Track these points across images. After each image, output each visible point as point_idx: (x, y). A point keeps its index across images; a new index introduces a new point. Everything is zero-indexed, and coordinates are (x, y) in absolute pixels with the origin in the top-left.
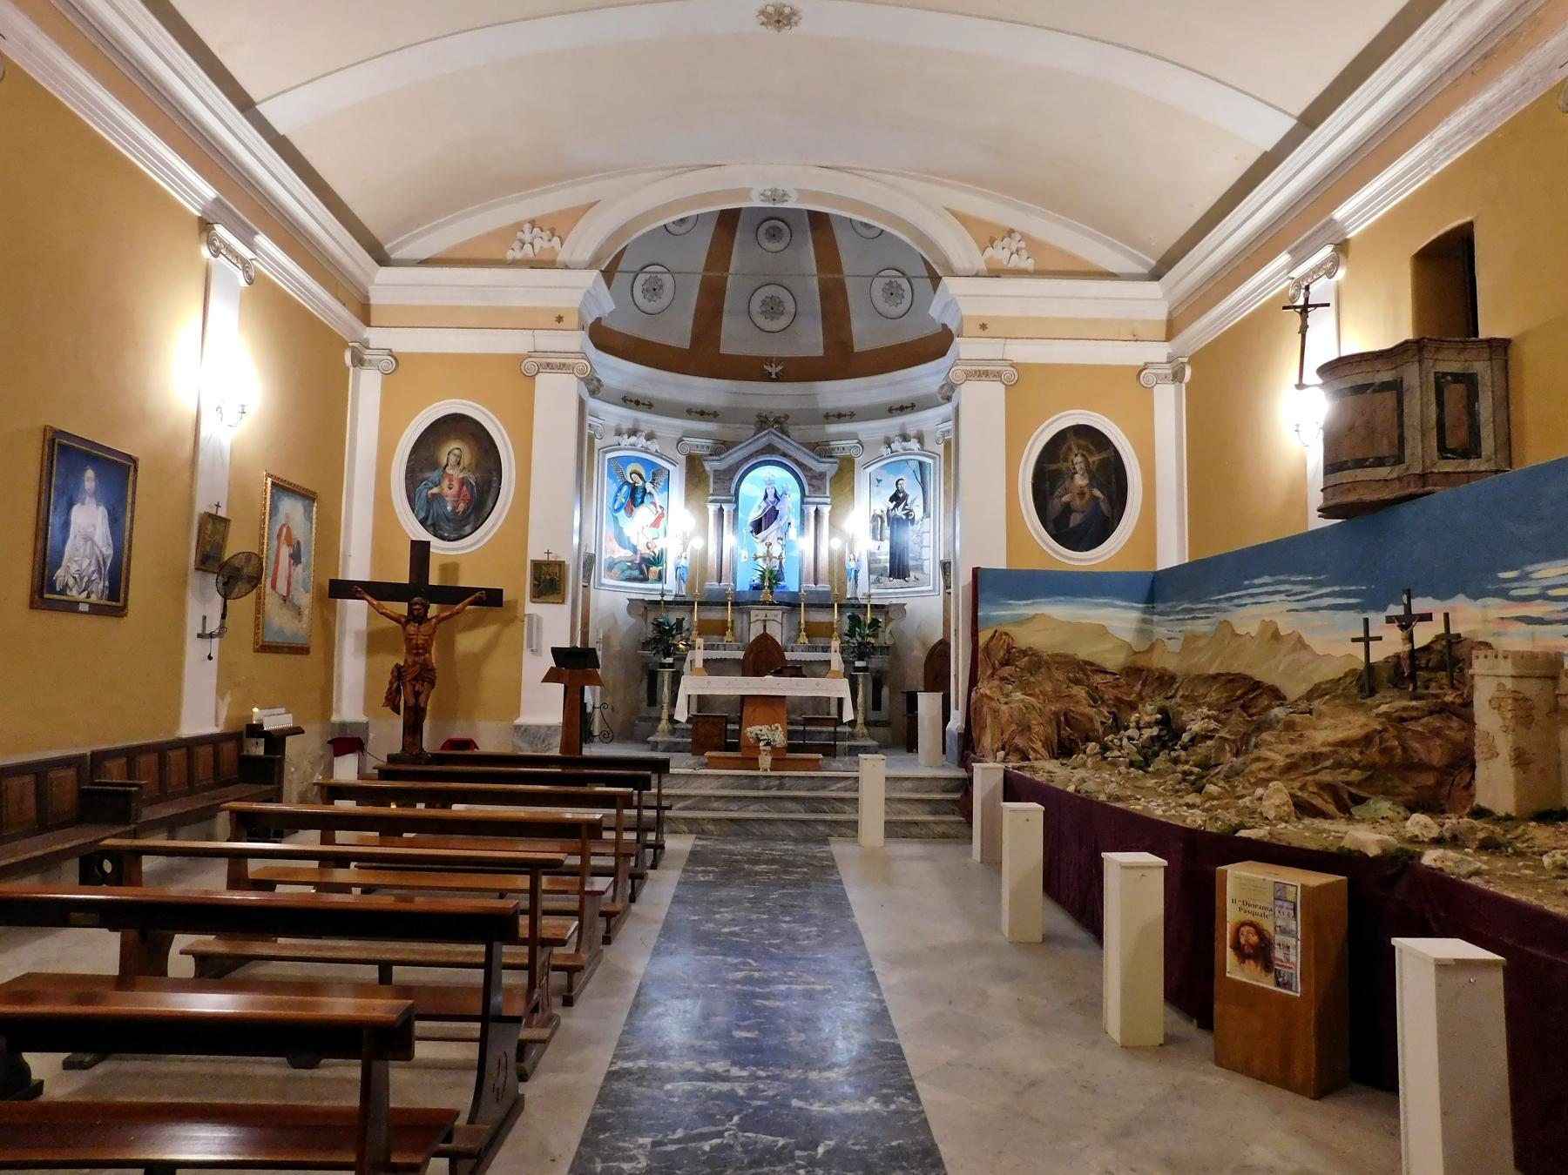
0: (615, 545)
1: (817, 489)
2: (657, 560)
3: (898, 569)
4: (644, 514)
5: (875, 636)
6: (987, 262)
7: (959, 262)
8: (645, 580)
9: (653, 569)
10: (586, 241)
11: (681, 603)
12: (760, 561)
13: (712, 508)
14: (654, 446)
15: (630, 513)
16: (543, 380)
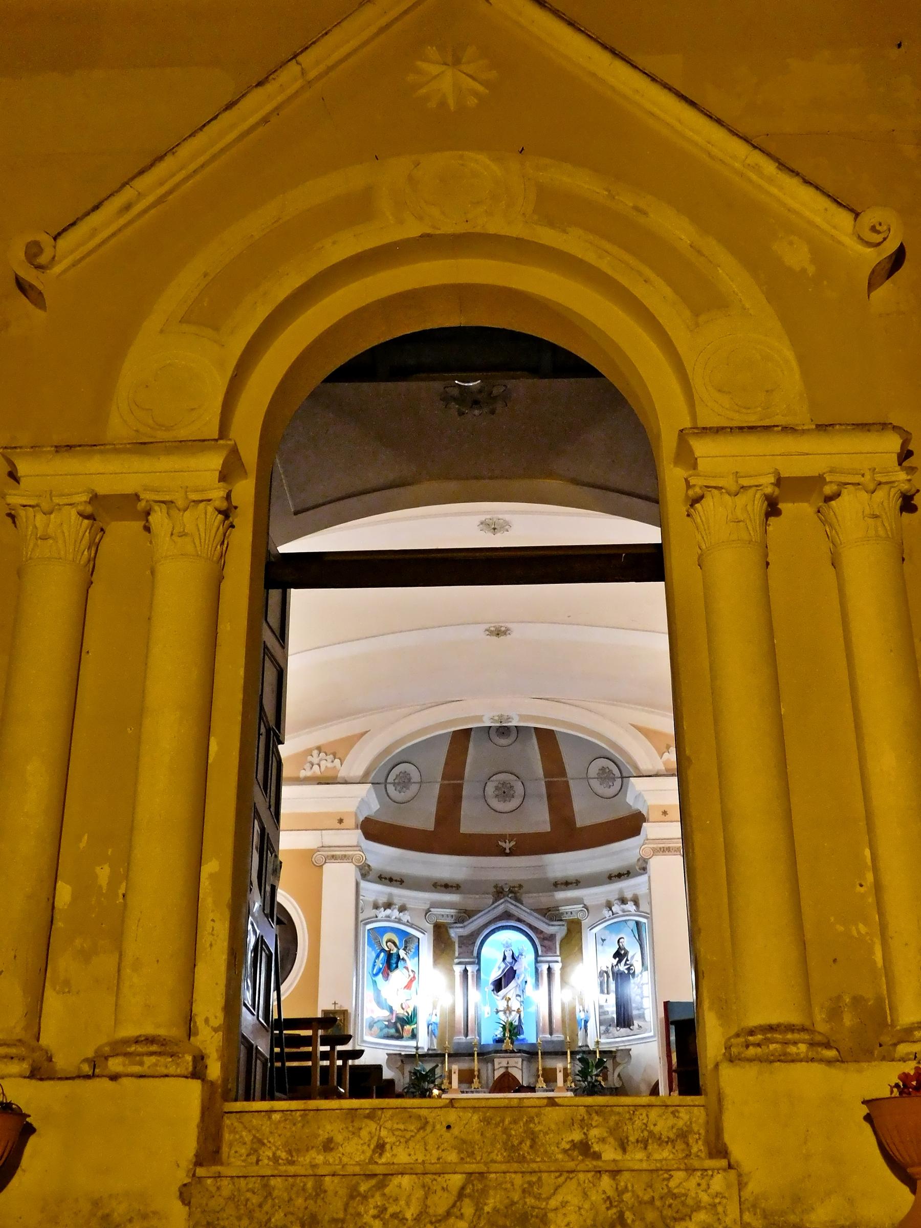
0: (374, 1005)
1: (549, 950)
2: (410, 1019)
3: (624, 1019)
4: (399, 976)
5: (605, 1079)
6: (665, 763)
7: (645, 765)
8: (400, 1037)
9: (407, 1027)
10: (358, 762)
11: (434, 1056)
12: (501, 1014)
13: (458, 969)
14: (405, 917)
15: (386, 977)
16: (330, 869)
